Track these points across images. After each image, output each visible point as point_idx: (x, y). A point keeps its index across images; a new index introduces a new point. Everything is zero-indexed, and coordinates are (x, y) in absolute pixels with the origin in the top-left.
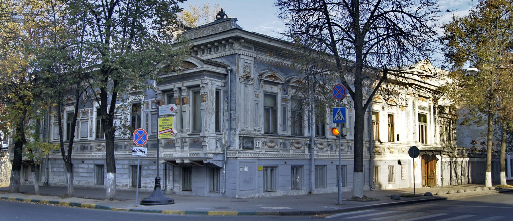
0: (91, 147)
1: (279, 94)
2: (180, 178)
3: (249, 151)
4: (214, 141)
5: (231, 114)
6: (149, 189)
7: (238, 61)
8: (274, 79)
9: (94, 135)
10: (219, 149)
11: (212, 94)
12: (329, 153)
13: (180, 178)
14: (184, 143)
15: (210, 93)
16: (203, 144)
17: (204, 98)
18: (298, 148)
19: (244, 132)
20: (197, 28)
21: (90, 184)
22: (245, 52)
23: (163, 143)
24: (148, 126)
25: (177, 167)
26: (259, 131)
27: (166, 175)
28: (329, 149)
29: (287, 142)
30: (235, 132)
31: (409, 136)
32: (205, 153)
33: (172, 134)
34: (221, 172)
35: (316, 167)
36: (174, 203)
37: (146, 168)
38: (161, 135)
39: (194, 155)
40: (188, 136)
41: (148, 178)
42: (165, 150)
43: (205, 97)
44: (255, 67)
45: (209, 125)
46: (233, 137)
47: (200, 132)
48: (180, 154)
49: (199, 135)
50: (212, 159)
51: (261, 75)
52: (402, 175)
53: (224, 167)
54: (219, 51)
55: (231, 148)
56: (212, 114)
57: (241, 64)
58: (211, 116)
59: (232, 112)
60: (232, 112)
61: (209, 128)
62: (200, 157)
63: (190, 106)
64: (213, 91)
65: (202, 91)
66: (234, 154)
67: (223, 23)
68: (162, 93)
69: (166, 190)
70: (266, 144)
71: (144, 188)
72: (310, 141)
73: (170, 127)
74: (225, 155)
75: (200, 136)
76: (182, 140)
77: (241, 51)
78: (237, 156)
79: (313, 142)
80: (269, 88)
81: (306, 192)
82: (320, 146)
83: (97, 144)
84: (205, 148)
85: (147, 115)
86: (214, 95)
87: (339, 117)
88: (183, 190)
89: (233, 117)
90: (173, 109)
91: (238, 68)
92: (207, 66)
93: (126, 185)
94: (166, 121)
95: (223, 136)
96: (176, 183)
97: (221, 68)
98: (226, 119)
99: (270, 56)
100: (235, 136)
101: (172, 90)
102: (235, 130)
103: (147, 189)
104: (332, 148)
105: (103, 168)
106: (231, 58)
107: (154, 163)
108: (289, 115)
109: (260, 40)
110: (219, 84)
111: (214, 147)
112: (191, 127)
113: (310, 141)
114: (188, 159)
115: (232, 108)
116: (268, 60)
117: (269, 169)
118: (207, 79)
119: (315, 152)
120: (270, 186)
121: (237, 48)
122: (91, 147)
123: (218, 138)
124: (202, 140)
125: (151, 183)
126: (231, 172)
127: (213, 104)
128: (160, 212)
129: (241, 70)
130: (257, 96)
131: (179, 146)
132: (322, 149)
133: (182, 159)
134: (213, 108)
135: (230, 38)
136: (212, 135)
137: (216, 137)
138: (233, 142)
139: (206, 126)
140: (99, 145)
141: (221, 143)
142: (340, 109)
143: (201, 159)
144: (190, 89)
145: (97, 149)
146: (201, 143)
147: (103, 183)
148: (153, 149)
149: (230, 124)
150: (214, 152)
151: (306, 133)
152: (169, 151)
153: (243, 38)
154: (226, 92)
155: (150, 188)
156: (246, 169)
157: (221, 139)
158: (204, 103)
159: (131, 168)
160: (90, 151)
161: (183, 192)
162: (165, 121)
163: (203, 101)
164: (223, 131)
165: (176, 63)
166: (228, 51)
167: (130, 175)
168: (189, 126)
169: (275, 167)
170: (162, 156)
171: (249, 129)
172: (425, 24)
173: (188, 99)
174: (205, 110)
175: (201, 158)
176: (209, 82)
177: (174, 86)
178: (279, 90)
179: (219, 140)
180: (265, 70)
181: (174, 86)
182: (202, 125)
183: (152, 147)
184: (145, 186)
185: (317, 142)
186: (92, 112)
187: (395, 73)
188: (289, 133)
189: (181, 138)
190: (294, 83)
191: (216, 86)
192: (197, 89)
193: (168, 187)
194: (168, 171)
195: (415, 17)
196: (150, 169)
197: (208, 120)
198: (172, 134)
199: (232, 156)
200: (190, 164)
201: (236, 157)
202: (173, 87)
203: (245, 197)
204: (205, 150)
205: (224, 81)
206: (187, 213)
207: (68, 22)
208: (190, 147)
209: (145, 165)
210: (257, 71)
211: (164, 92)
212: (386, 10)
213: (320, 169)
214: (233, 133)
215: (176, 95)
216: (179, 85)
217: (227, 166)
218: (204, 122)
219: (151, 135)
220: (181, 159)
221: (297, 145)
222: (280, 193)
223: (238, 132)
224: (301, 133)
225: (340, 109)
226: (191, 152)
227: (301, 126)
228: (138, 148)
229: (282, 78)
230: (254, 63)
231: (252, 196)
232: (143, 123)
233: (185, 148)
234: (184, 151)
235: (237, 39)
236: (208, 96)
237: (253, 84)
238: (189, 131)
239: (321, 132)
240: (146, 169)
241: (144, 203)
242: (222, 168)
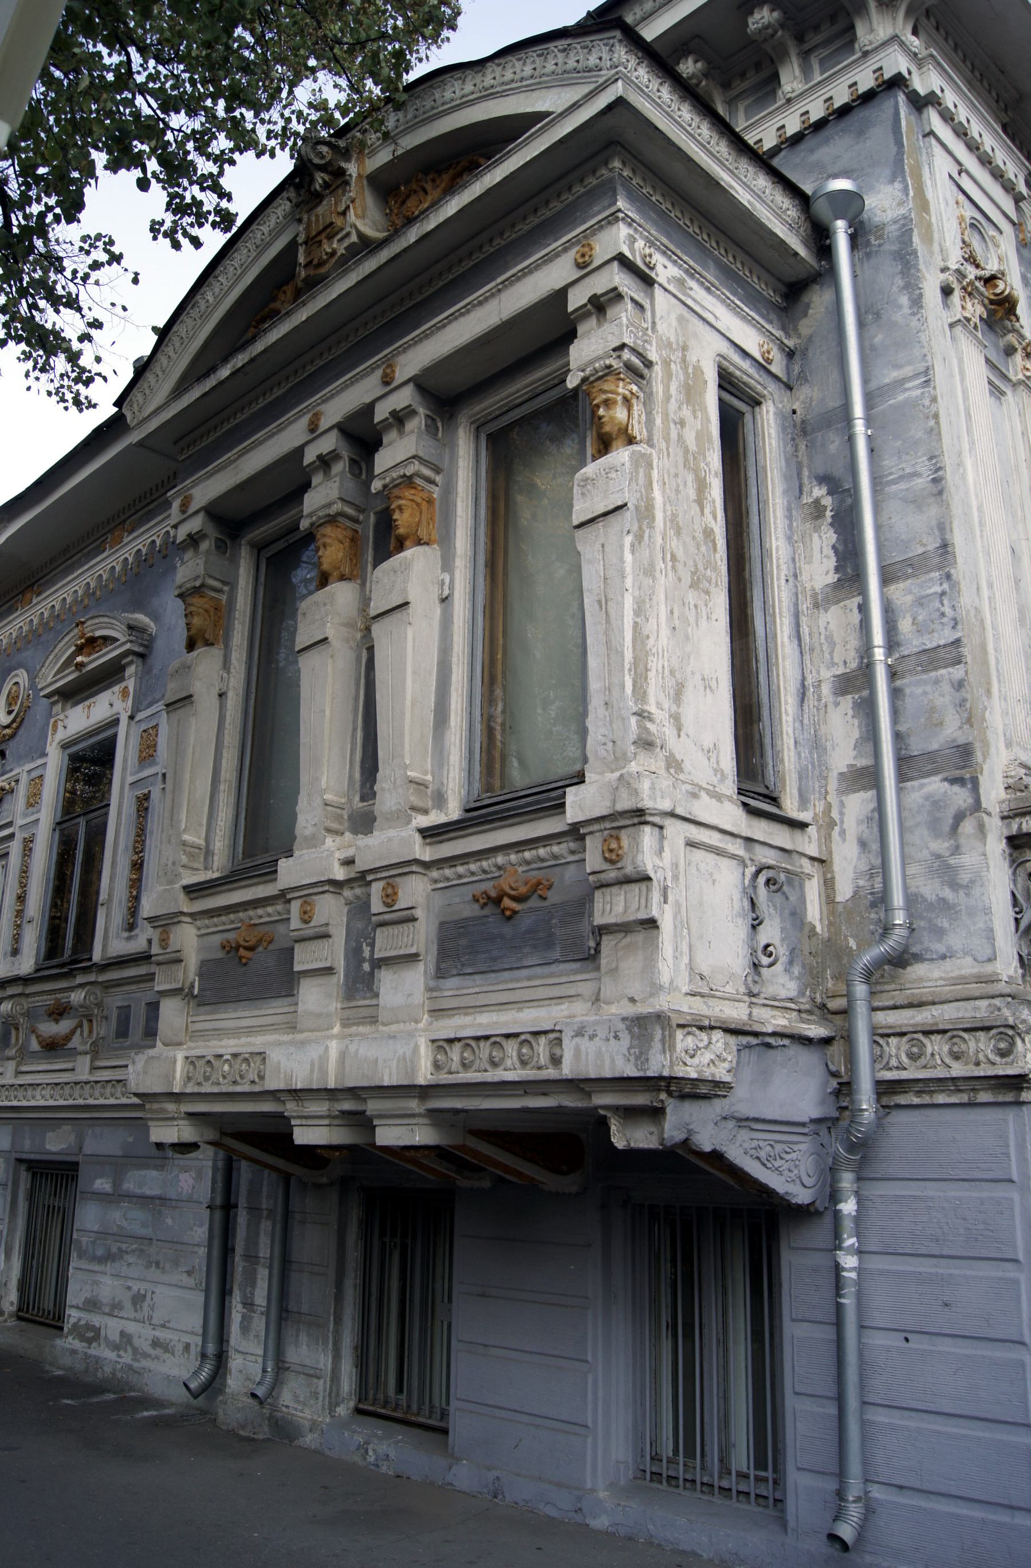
2: (339, 1297)
6: (110, 1355)
11: (691, 393)
13: (339, 1297)
14: (381, 935)
15: (669, 375)
17: (608, 403)
23: (192, 960)
24: (140, 880)
25: (318, 1186)
27: (227, 1251)
30: (960, 796)
37: (102, 1184)
39: (485, 1047)
40: (427, 854)
41: (109, 1268)
43: (627, 401)
45: (678, 694)
46: (941, 846)
48: (334, 1048)
50: (718, 1107)
53: (848, 1207)
55: (918, 970)
56: (694, 585)
58: (692, 597)
61: (676, 720)
62: (567, 1070)
63: (447, 565)
64: (698, 370)
66: (982, 1045)
68: (213, 532)
69: (221, 1391)
71: (83, 1338)
74: (851, 1058)
75: (573, 813)
76: (360, 908)
84: (632, 965)
86: (704, 409)
88: (359, 1411)
95: (809, 843)
96: (303, 1338)
100: (968, 826)
103: (94, 1351)
114: (413, 1105)
123: (768, 857)
125: (128, 1304)
126: (944, 1268)
131: (329, 971)
134: (708, 533)
136: (706, 809)
137: (749, 840)
138: (944, 905)
139: (640, 693)
143: (570, 1101)
146: (583, 904)
150: (736, 1013)
155: (116, 1347)
159: (25, 1179)
161: (363, 1432)
163: (605, 445)
164: (804, 802)
165: (291, 44)
167: (11, 1231)
170: (169, 1077)
173: (430, 502)
175: (578, 1085)
182: (594, 685)
184: (89, 1327)
189: (348, 882)
191: (725, 348)
193: (235, 1362)
194: (242, 1218)
196: (129, 1196)
199: (958, 1070)
200: (442, 1167)
204: (635, 989)
208: (441, 974)
209: (102, 1160)
218: (613, 650)
220: (347, 1106)
233: (387, 981)
234: (373, 1020)
236: (649, 396)
238: (440, 800)
240: (101, 1197)
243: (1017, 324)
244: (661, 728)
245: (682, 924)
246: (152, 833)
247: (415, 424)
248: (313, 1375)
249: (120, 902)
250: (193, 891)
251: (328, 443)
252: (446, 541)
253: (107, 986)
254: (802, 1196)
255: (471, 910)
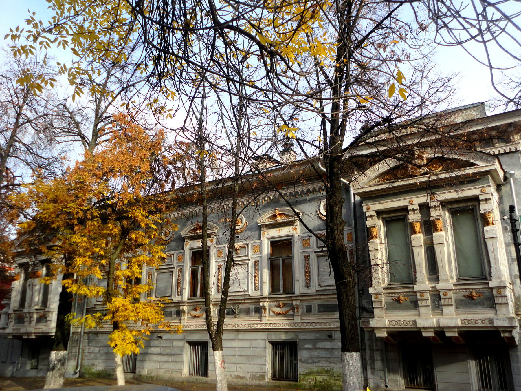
21: (173, 375)
40: (453, 288)
42: (389, 313)
83: (192, 307)
85: (307, 258)
93: (262, 377)
101: (405, 210)
107: (328, 338)
147: (205, 373)
148: (325, 313)
152: (400, 316)
181: (411, 203)
183: (322, 310)
186: (181, 258)
196: (319, 348)
202: (407, 204)
208: (456, 308)
216: (421, 199)
219: (317, 291)
232: (299, 271)
246: (312, 265)
249: (302, 280)
250: (384, 289)
253: (301, 300)
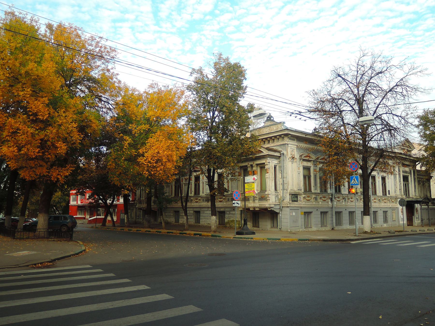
0: (191, 200)
1: (311, 167)
3: (296, 203)
4: (274, 197)
5: (283, 180)
7: (287, 148)
8: (308, 158)
9: (193, 193)
10: (277, 201)
11: (272, 169)
12: (344, 203)
16: (268, 198)
18: (325, 201)
19: (292, 191)
20: (259, 128)
22: (293, 143)
26: (301, 190)
28: (343, 201)
29: (318, 197)
31: (397, 192)
32: (269, 204)
33: (254, 193)
34: (278, 216)
35: (336, 212)
36: (255, 234)
38: (247, 194)
44: (297, 151)
45: (271, 187)
47: (266, 191)
49: (265, 193)
51: (301, 156)
52: (393, 218)
53: (280, 213)
54: (275, 142)
57: (289, 150)
59: (284, 179)
60: (284, 179)
63: (258, 176)
65: (266, 167)
66: (286, 205)
67: (276, 125)
70: (305, 198)
72: (332, 195)
73: (253, 189)
77: (289, 142)
78: (289, 206)
79: (333, 197)
80: (306, 164)
81: (330, 228)
82: (338, 199)
87: (355, 182)
89: (285, 182)
90: (255, 179)
91: (287, 152)
92: (269, 152)
94: (250, 186)
97: (277, 153)
98: (281, 183)
99: (306, 144)
102: (287, 190)
104: (345, 200)
105: (199, 213)
106: (282, 147)
108: (318, 180)
109: (300, 135)
110: (276, 162)
111: (274, 200)
112: (259, 188)
113: (332, 195)
115: (284, 177)
116: (304, 147)
117: (307, 214)
118: (269, 160)
119: (335, 203)
120: (307, 225)
121: (286, 141)
122: (191, 200)
124: (267, 196)
127: (273, 174)
128: (252, 238)
129: (289, 153)
130: (299, 169)
132: (339, 201)
133: (254, 208)
135: (282, 134)
136: (273, 193)
138: (286, 197)
139: (269, 188)
140: (197, 199)
141: (278, 198)
142: (355, 177)
144: (258, 166)
145: (195, 201)
146: (267, 198)
149: (284, 186)
150: (274, 203)
151: (329, 191)
153: (290, 134)
154: (280, 167)
156: (294, 214)
157: (278, 196)
158: (268, 174)
160: (190, 203)
161: (253, 228)
162: (249, 186)
163: (267, 173)
164: (279, 191)
166: (281, 142)
168: (258, 188)
169: (311, 212)
171: (295, 189)
172: (407, 121)
174: (268, 178)
176: (270, 161)
177: (248, 164)
178: (312, 164)
179: (277, 196)
180: (303, 152)
181: (248, 164)
185: (336, 197)
187: (215, 118)
188: (319, 191)
190: (320, 159)
192: (262, 165)
195: (400, 117)
197: (270, 184)
198: (254, 193)
201: (288, 207)
203: (294, 231)
205: (278, 160)
206: (300, 240)
207: (117, 116)
209: (228, 211)
210: (298, 154)
211: (241, 167)
212: (381, 113)
213: (338, 214)
214: (286, 192)
215: (249, 169)
216: (251, 163)
217: (282, 212)
218: (268, 185)
221: (323, 199)
222: (314, 229)
223: (289, 191)
224: (326, 191)
225: (355, 177)
226: (260, 204)
227: (326, 187)
228: (236, 202)
229: (314, 157)
230: (297, 149)
231: (298, 230)
235: (286, 135)
237: (296, 162)
238: (258, 191)
239: (338, 190)
241: (238, 233)
242: (279, 213)
243: (317, 114)
244: (270, 189)
245: (271, 199)
247: (256, 167)
248: (250, 224)
251: (249, 166)
252: (258, 174)
254: (278, 212)
255: (260, 197)
